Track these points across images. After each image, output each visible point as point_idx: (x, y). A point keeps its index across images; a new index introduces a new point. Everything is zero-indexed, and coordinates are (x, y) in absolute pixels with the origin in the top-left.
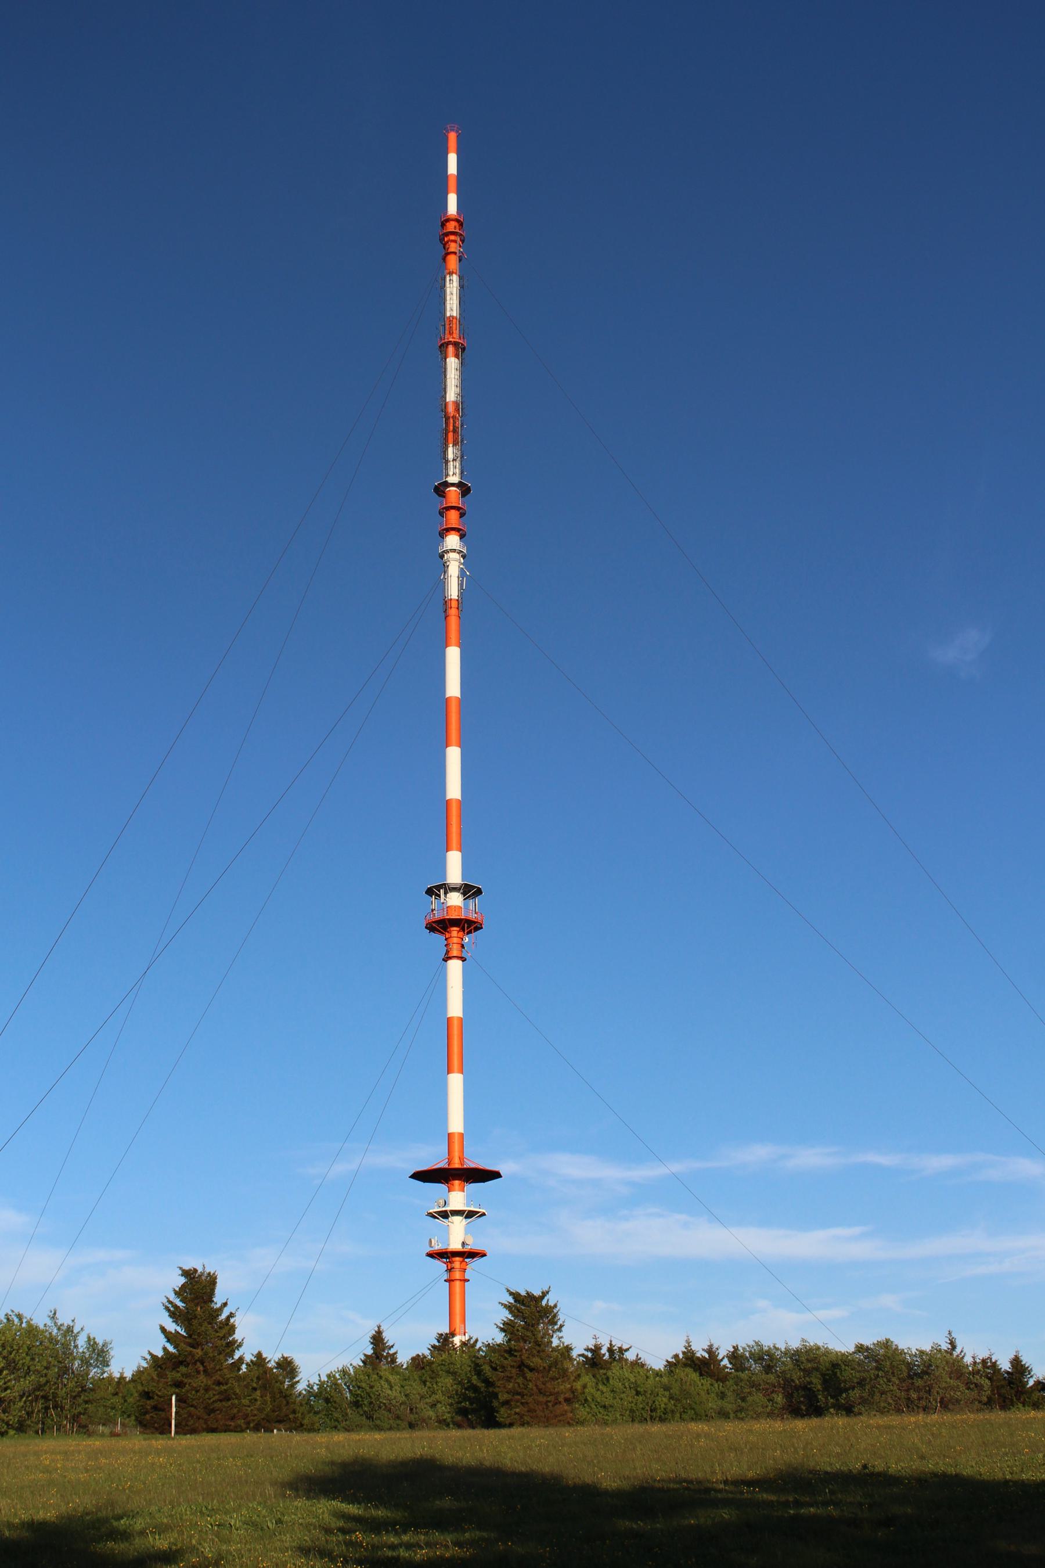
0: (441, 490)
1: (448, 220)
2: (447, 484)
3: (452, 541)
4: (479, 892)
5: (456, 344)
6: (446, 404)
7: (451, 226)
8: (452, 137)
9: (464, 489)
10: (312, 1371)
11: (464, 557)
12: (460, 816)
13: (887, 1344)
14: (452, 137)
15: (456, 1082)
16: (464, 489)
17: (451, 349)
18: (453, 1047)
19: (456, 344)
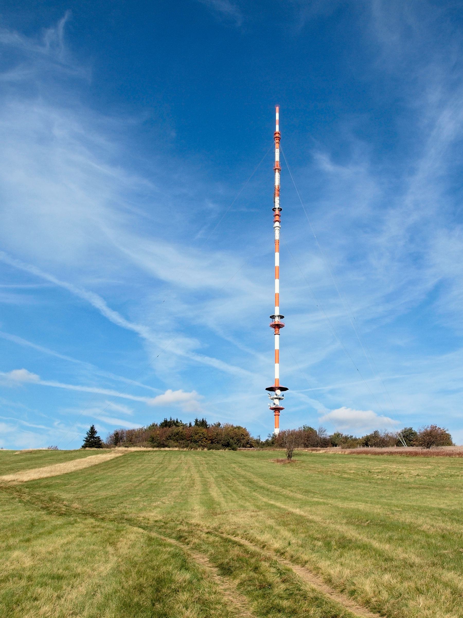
0: (274, 210)
1: (276, 133)
2: (275, 208)
3: (277, 224)
4: (271, 317)
5: (278, 169)
6: (275, 186)
7: (277, 212)
8: (277, 108)
9: (280, 210)
10: (263, 440)
11: (280, 228)
12: (140, 451)
13: (434, 428)
14: (277, 108)
15: (277, 281)
16: (280, 210)
17: (277, 170)
18: (278, 273)
19: (278, 169)
